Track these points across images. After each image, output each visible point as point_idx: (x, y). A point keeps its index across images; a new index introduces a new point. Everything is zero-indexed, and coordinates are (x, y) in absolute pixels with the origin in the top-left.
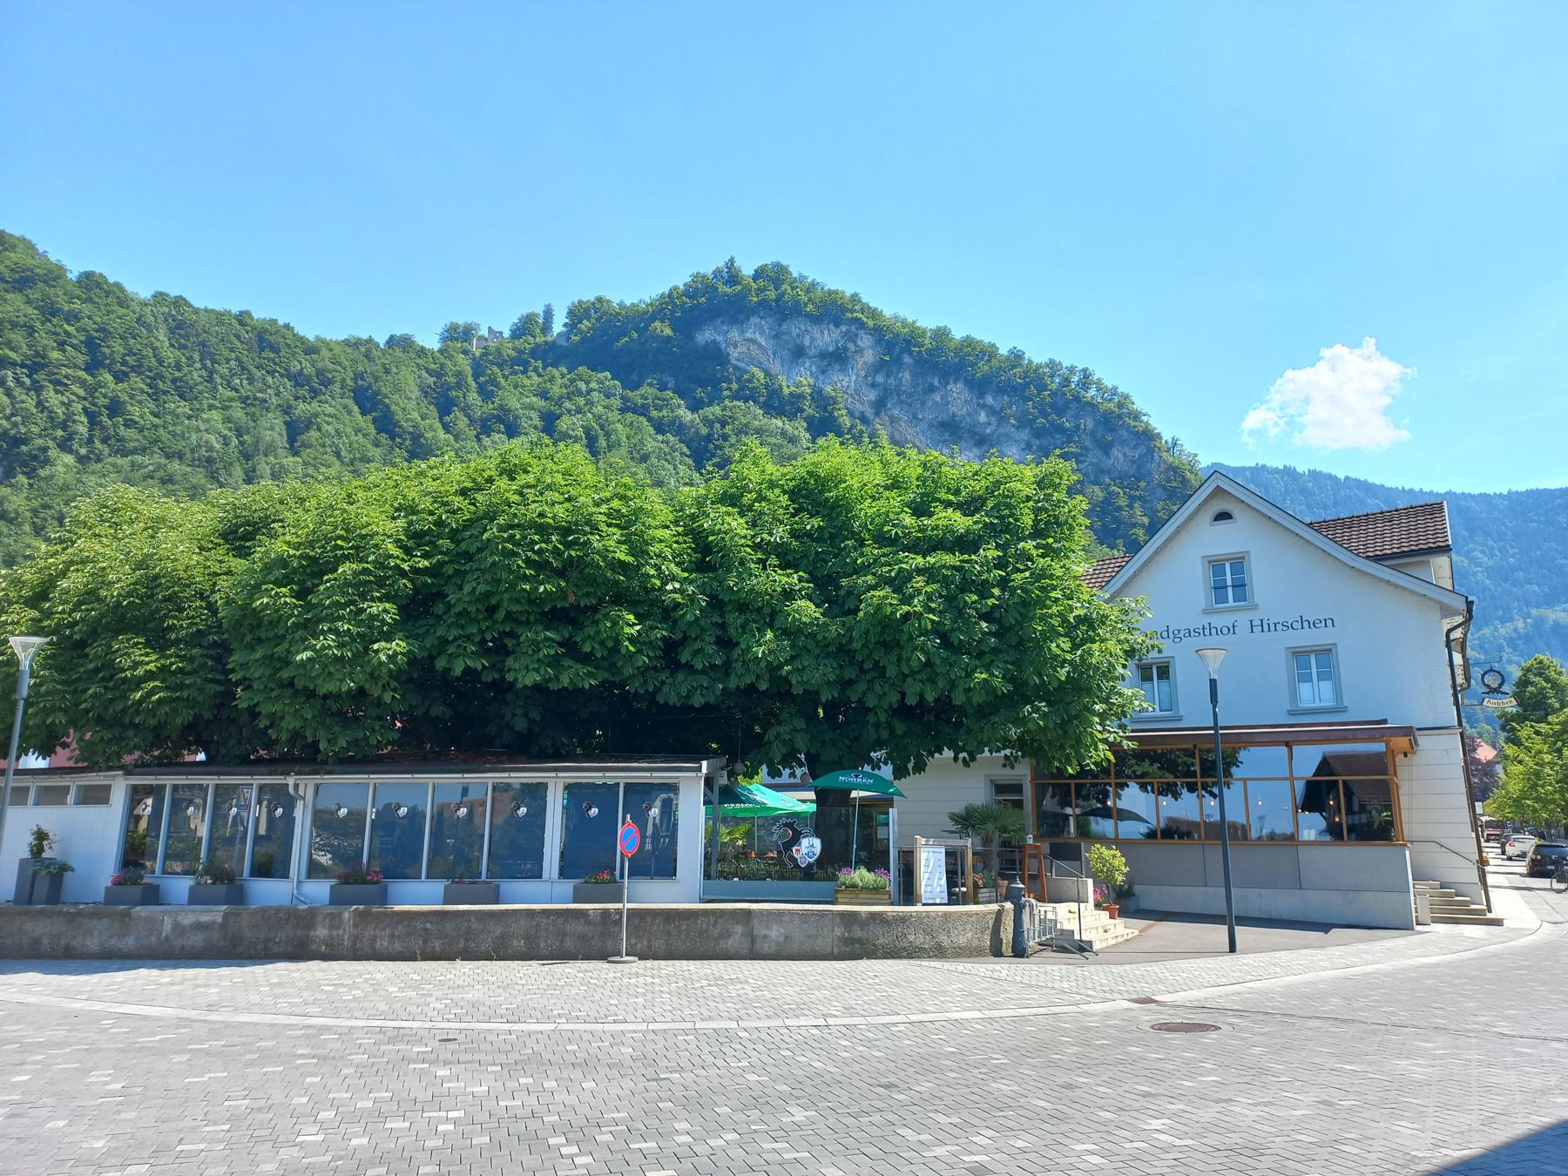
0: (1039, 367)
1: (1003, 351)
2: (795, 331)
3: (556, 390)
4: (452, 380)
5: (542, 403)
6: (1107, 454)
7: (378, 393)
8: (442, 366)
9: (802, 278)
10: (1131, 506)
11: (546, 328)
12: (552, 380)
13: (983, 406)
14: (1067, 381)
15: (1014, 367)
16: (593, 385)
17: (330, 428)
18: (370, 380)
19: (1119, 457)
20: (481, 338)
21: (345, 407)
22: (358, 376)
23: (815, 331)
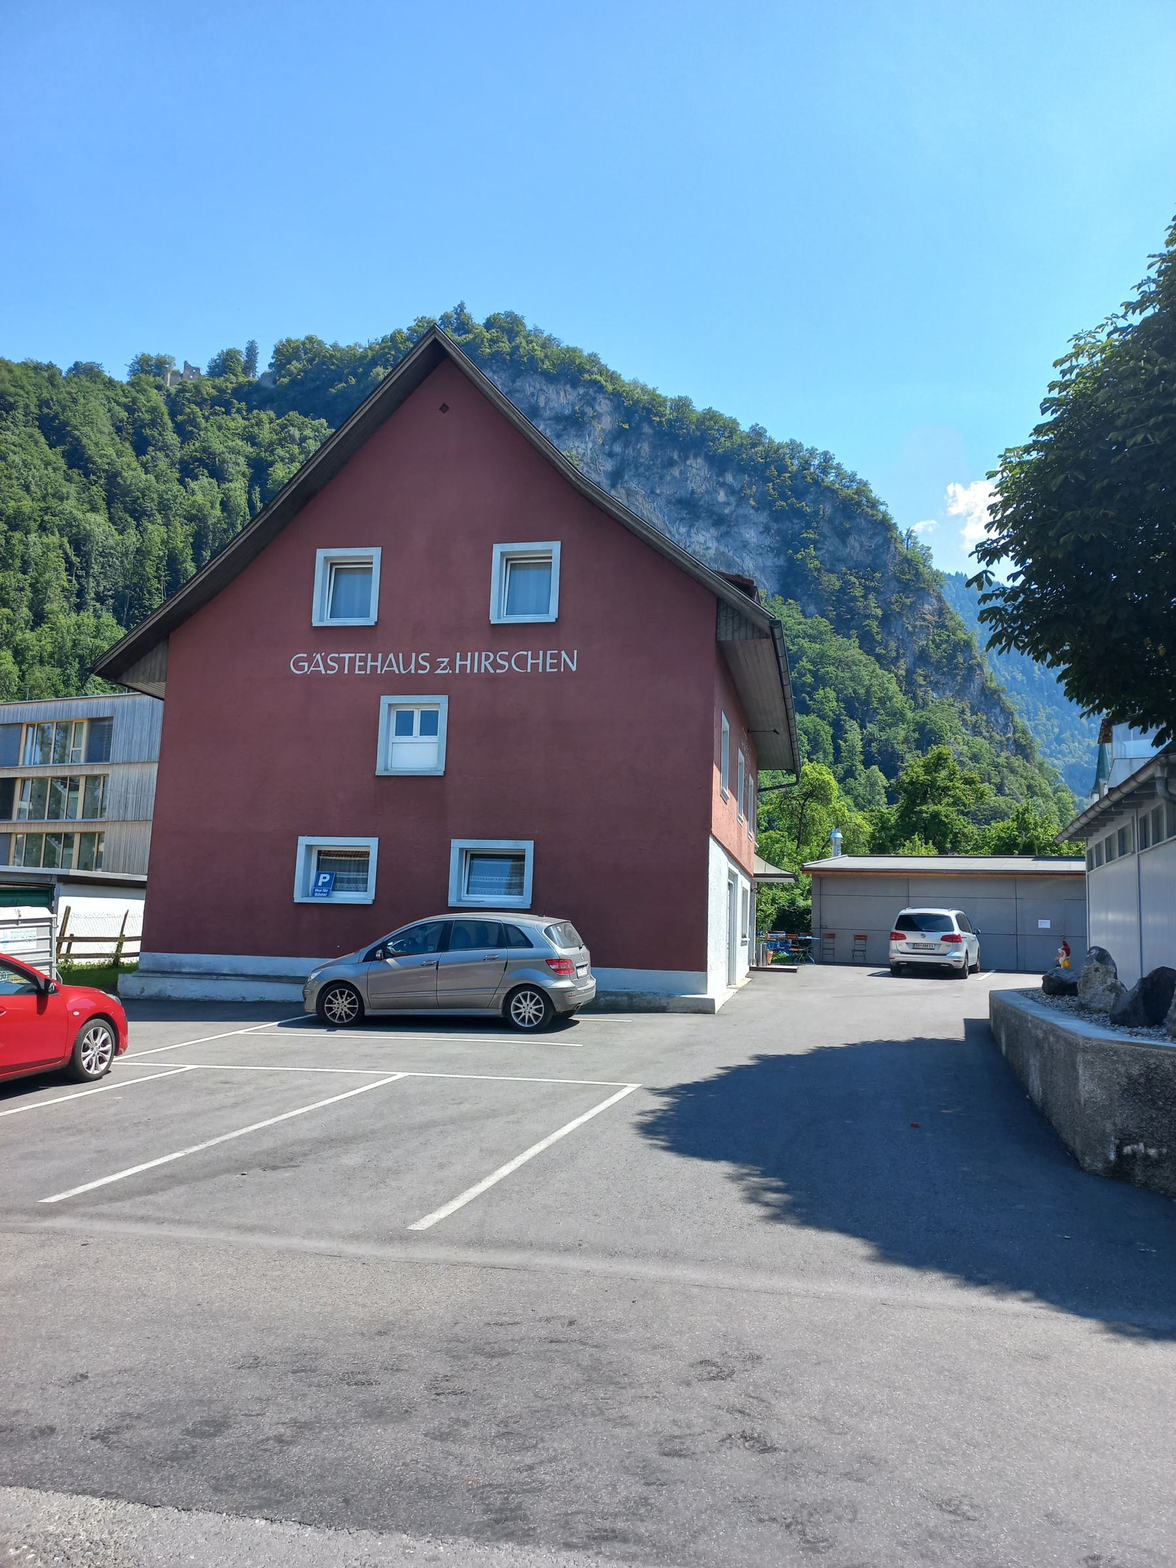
0: (780, 446)
1: (745, 427)
2: (529, 390)
3: (266, 434)
4: (147, 417)
5: (249, 449)
6: (844, 542)
7: (66, 424)
8: (134, 400)
9: (538, 332)
10: (865, 597)
11: (250, 366)
12: (259, 423)
13: (723, 485)
14: (806, 465)
15: (754, 445)
16: (308, 432)
17: (17, 459)
18: (57, 408)
19: (855, 547)
20: (176, 374)
21: (31, 436)
22: (43, 403)
23: (551, 391)
